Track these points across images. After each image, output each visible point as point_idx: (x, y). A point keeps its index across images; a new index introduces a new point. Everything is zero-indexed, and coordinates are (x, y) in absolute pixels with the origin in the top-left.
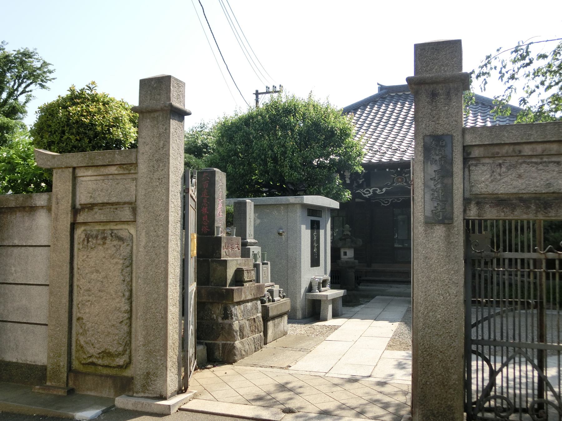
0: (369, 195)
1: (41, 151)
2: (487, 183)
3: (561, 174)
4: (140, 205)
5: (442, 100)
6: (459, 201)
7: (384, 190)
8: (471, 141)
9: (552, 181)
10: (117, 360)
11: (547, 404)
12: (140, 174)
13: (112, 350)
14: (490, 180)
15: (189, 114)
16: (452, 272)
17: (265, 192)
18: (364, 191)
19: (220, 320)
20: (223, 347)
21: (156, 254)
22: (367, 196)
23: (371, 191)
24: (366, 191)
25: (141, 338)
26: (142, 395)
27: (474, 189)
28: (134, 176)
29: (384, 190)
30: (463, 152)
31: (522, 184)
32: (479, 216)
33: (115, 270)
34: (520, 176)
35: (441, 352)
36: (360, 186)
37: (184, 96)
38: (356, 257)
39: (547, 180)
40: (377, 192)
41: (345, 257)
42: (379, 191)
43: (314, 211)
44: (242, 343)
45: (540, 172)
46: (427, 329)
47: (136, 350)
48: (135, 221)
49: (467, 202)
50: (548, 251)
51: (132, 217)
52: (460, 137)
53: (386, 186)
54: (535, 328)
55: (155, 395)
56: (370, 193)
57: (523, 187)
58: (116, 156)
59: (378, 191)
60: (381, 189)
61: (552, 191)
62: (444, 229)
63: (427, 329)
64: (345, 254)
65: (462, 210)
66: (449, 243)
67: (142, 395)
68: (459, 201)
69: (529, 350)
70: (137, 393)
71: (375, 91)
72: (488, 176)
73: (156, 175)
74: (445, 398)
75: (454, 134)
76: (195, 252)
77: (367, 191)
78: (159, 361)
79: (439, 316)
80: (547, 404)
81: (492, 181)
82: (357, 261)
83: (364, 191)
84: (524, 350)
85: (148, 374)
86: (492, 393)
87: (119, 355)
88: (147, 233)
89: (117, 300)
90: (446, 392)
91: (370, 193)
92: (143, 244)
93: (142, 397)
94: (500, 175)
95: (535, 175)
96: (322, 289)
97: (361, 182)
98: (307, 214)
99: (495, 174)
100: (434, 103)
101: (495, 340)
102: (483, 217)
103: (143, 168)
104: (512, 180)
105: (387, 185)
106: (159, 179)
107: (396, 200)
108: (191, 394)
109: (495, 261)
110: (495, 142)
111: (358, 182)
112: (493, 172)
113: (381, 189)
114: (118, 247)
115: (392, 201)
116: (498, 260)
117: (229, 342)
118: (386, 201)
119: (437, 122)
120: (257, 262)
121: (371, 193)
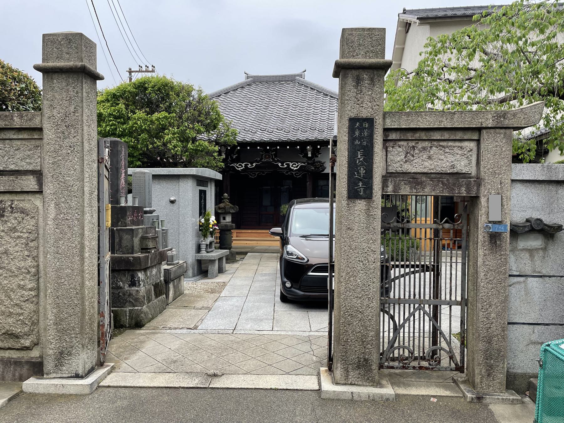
2: (402, 163)
4: (45, 172)
5: (367, 85)
6: (378, 179)
7: (254, 164)
8: (391, 125)
9: (455, 163)
10: (22, 341)
11: (440, 350)
12: (45, 140)
13: (18, 330)
14: (404, 160)
15: (102, 78)
16: (371, 241)
19: (126, 288)
20: (130, 313)
21: (69, 227)
22: (239, 169)
23: (243, 165)
25: (51, 316)
26: (54, 375)
27: (390, 168)
28: (38, 143)
29: (254, 164)
31: (431, 165)
32: (394, 192)
33: (16, 245)
34: (430, 158)
35: (360, 312)
36: (233, 161)
37: (95, 59)
38: (233, 221)
39: (452, 162)
41: (224, 221)
43: (201, 181)
44: (148, 307)
45: (446, 154)
46: (348, 292)
47: (45, 329)
48: (42, 192)
49: (385, 179)
50: (445, 223)
51: (37, 187)
52: (381, 120)
53: (256, 161)
54: (443, 288)
55: (70, 375)
57: (432, 167)
58: (15, 118)
59: (249, 166)
60: (252, 164)
61: (456, 171)
62: (365, 203)
63: (348, 292)
64: (224, 219)
65: (380, 186)
66: (369, 216)
67: (54, 375)
68: (378, 179)
69: (427, 306)
70: (47, 374)
71: (242, 79)
72: (403, 157)
73: (67, 142)
74: (363, 353)
75: (377, 117)
76: (110, 222)
78: (74, 339)
79: (359, 281)
80: (440, 350)
81: (406, 161)
82: (234, 225)
84: (422, 305)
85: (61, 353)
86: (396, 345)
87: (27, 334)
88: (57, 205)
89: (21, 277)
90: (365, 347)
92: (52, 216)
93: (54, 378)
94: (413, 156)
95: (443, 157)
96: (209, 250)
97: (234, 157)
98: (195, 184)
99: (409, 155)
100: (359, 87)
101: (399, 298)
102: (398, 192)
103: (49, 134)
104: (423, 161)
106: (70, 147)
108: (109, 368)
109: (401, 231)
110: (412, 126)
111: (232, 158)
112: (407, 153)
113: (252, 164)
114: (20, 219)
116: (403, 229)
117: (136, 308)
119: (362, 105)
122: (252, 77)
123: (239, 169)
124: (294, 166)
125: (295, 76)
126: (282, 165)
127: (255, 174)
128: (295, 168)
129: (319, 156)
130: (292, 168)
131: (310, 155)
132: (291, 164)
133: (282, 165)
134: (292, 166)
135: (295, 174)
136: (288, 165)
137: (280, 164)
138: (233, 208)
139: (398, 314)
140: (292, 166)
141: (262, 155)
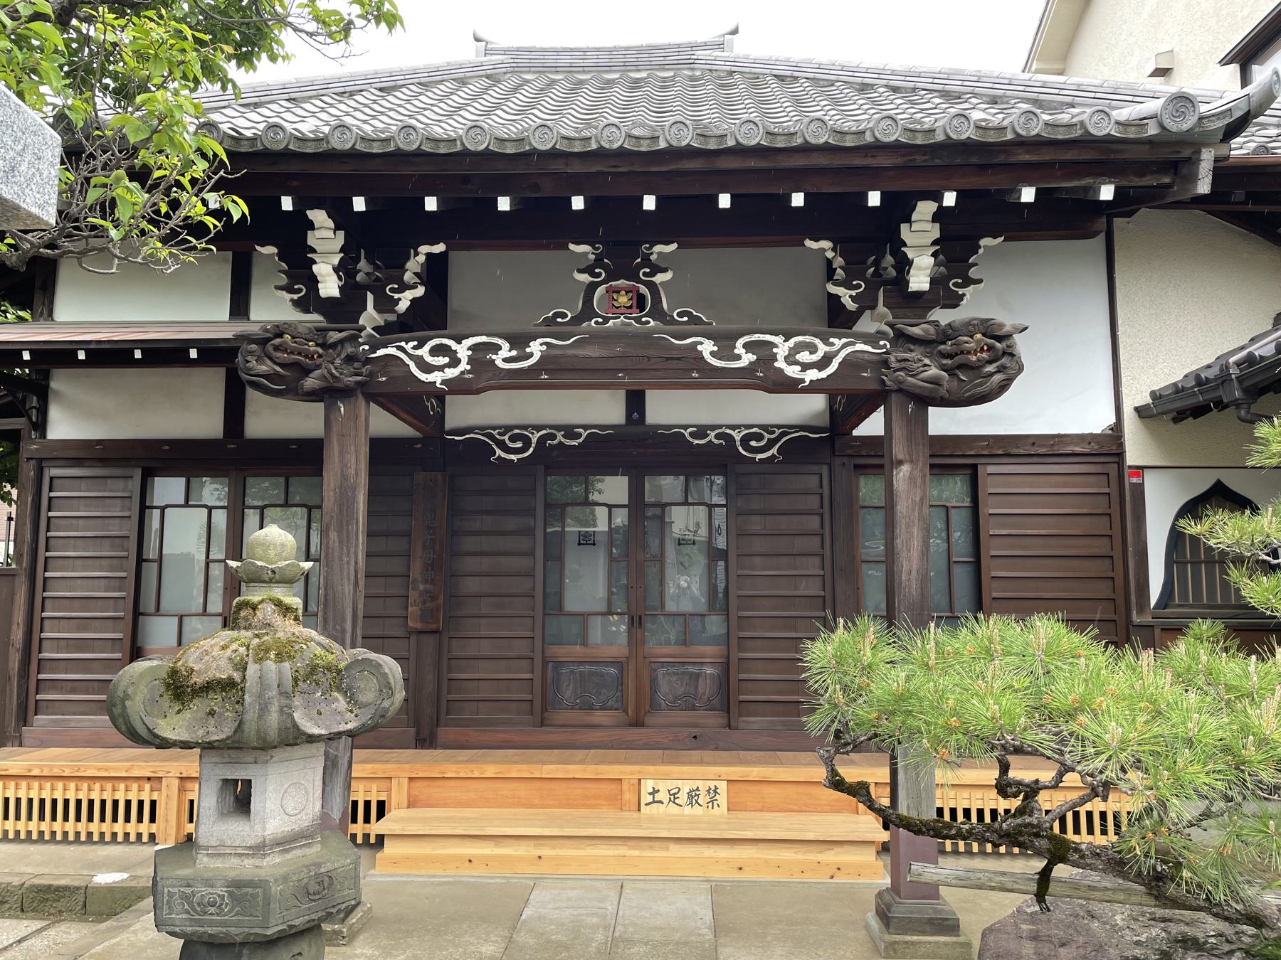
0: (451, 373)
1: (908, 938)
3: (1280, 437)
7: (536, 348)
17: (24, 364)
18: (424, 352)
22: (437, 377)
24: (435, 351)
29: (536, 348)
30: (296, 744)
40: (498, 359)
41: (237, 831)
42: (506, 351)
56: (455, 362)
60: (519, 341)
77: (438, 351)
83: (424, 352)
91: (455, 362)
97: (404, 301)
105: (550, 322)
107: (560, 437)
113: (519, 341)
115: (542, 440)
118: (514, 439)
120: (257, 666)
121: (464, 366)
122: (505, 51)
123: (437, 377)
124: (804, 357)
125: (693, 47)
126: (725, 352)
127: (527, 442)
128: (813, 375)
129: (969, 291)
130: (793, 371)
131: (919, 281)
132: (782, 348)
133: (725, 352)
134: (790, 360)
135: (745, 440)
136: (764, 353)
137: (707, 348)
138: (339, 680)
139: (503, 560)
140: (790, 360)
141: (592, 288)
